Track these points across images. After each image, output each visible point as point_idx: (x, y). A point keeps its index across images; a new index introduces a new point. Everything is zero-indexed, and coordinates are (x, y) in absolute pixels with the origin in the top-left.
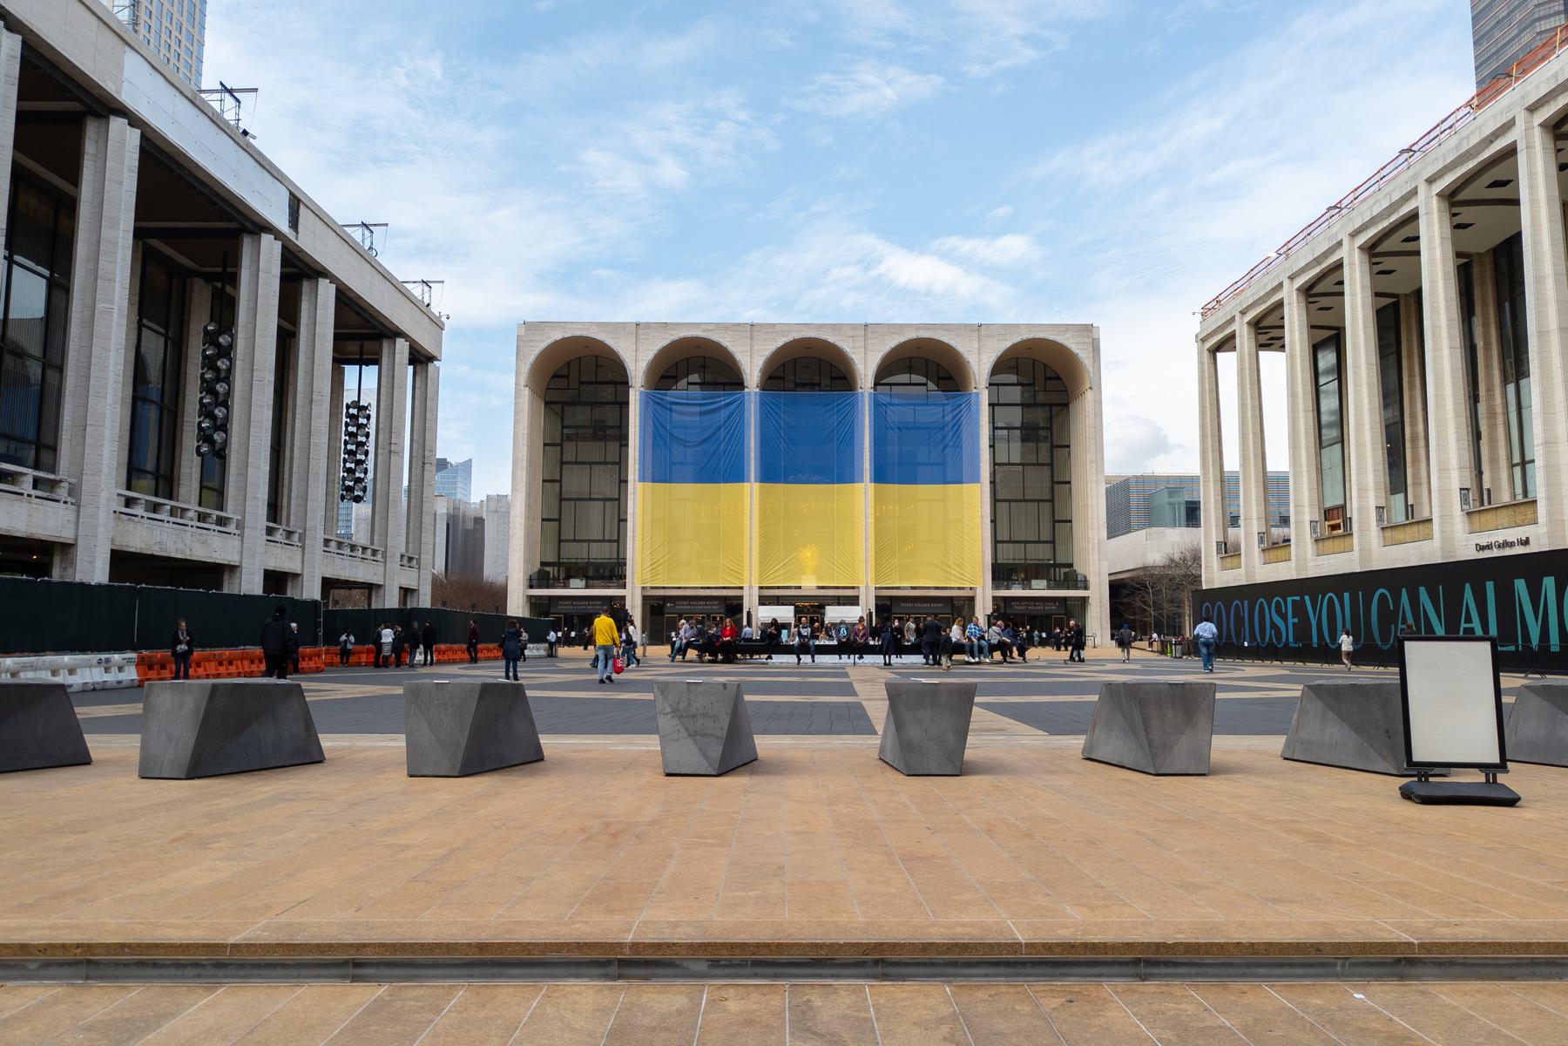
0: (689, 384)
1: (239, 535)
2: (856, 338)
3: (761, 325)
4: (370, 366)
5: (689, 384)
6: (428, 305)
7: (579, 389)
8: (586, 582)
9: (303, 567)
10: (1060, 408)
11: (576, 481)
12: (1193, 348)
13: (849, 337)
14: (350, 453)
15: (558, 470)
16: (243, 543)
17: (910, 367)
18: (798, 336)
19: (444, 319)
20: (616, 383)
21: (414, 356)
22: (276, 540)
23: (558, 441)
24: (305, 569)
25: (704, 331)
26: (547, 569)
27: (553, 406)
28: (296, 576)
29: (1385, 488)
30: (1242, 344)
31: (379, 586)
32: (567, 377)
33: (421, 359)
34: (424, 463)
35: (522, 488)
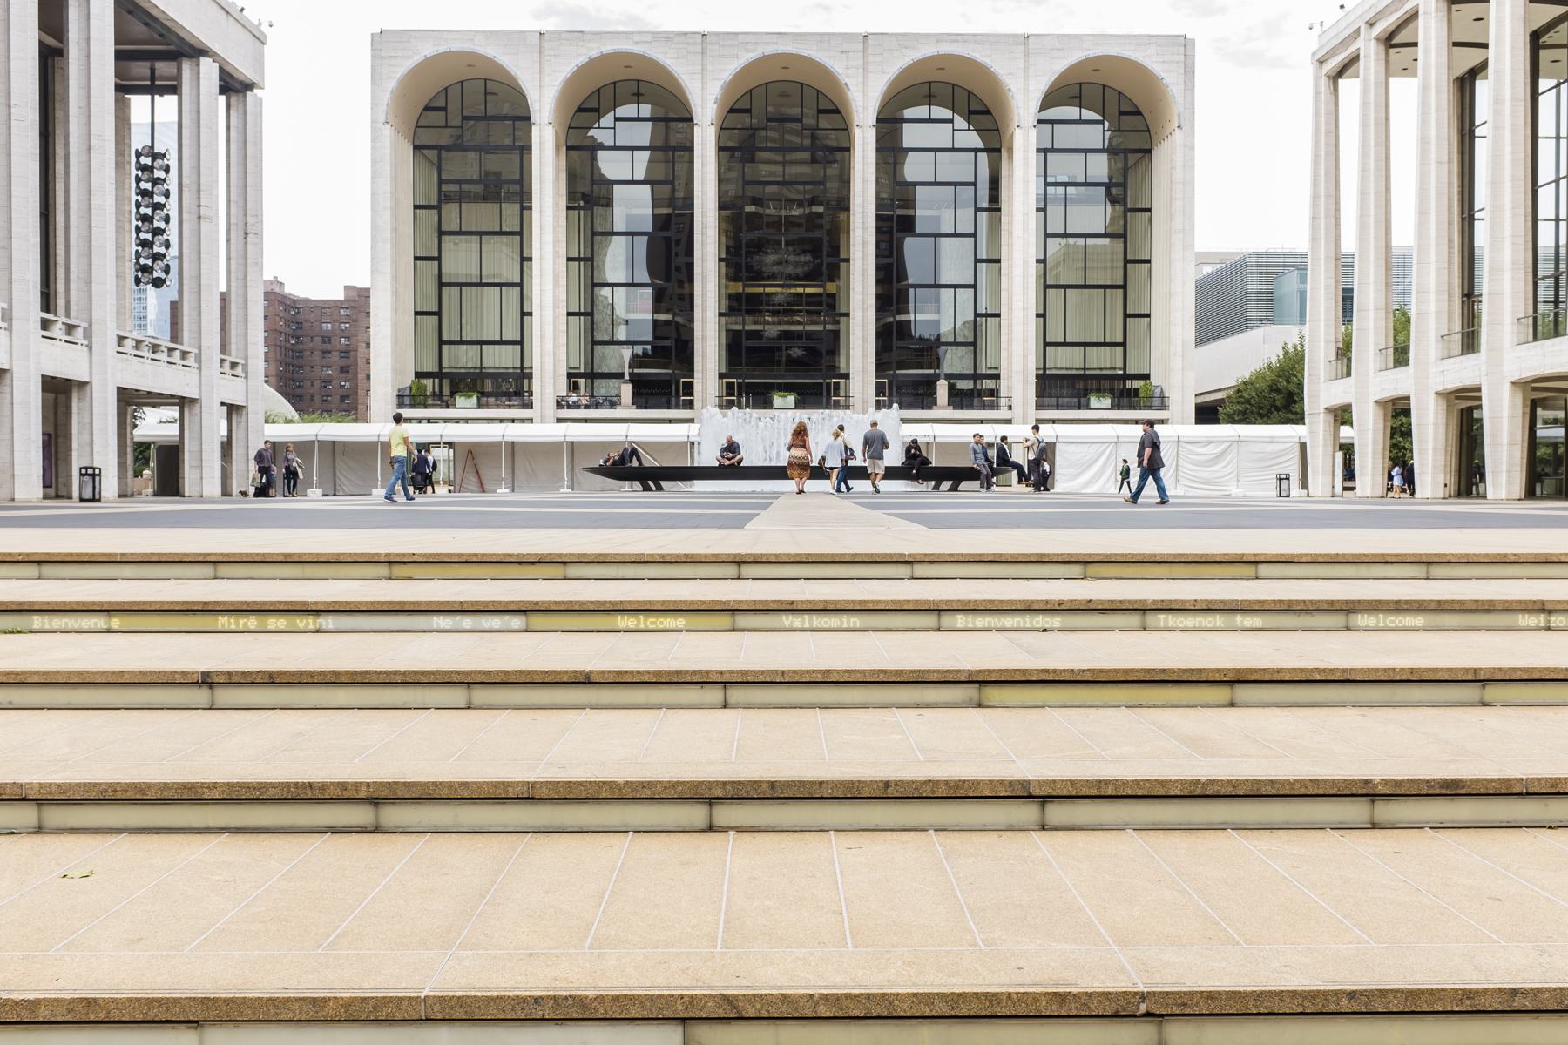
0: (617, 119)
1: (5, 329)
2: (851, 54)
3: (717, 34)
4: (165, 96)
5: (617, 119)
6: (242, 10)
7: (462, 127)
8: (478, 399)
9: (91, 374)
10: (1140, 155)
11: (460, 259)
12: (1309, 70)
13: (842, 52)
14: (145, 219)
15: (436, 241)
16: (11, 340)
17: (930, 96)
18: (769, 50)
19: (265, 28)
20: (515, 118)
21: (226, 82)
22: (54, 337)
23: (434, 202)
24: (94, 376)
25: (637, 43)
26: (423, 381)
27: (425, 152)
28: (82, 385)
29: (1525, 267)
30: (1367, 69)
31: (193, 401)
32: (444, 109)
33: (233, 86)
34: (246, 234)
35: (387, 268)
